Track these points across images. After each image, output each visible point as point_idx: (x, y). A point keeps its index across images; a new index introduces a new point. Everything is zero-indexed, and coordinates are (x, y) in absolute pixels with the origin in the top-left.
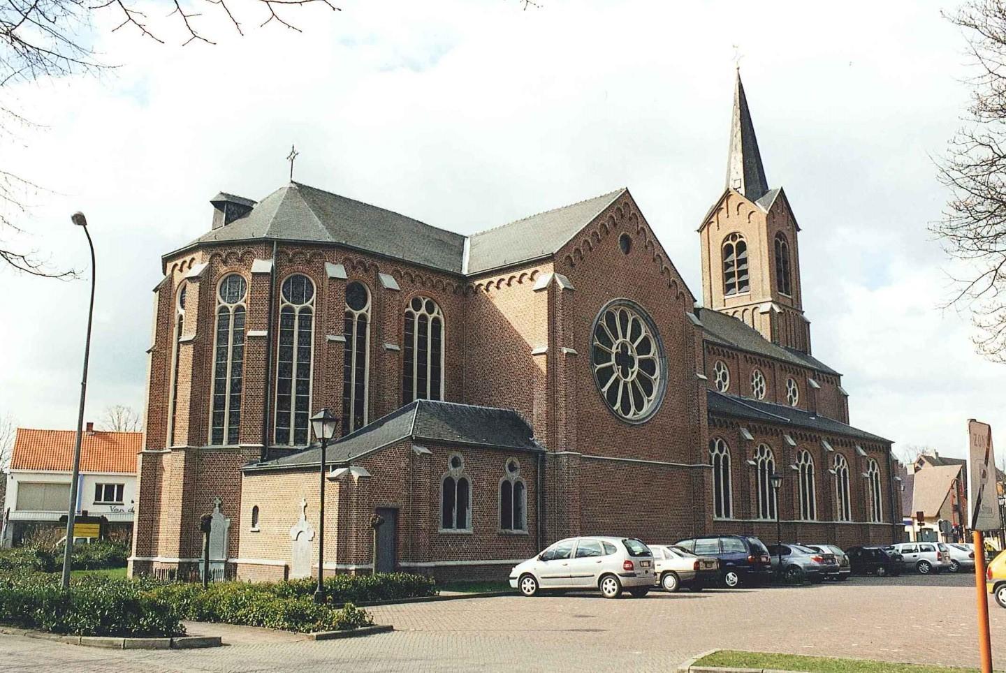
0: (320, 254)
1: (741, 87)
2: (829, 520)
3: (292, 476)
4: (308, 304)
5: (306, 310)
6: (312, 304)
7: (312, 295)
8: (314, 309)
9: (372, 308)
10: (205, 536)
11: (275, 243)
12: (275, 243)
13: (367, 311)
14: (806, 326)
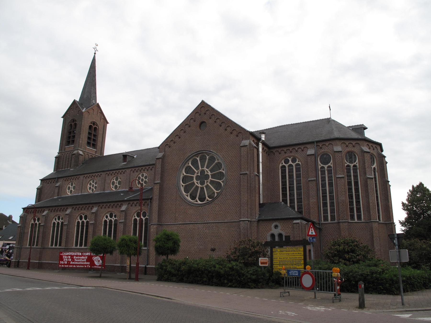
0: (331, 144)
1: (94, 57)
2: (393, 250)
3: (96, 286)
4: (355, 164)
5: (355, 166)
6: (331, 164)
7: (331, 160)
8: (358, 165)
9: (333, 162)
10: (289, 315)
11: (315, 142)
12: (315, 142)
13: (357, 163)
14: (379, 148)
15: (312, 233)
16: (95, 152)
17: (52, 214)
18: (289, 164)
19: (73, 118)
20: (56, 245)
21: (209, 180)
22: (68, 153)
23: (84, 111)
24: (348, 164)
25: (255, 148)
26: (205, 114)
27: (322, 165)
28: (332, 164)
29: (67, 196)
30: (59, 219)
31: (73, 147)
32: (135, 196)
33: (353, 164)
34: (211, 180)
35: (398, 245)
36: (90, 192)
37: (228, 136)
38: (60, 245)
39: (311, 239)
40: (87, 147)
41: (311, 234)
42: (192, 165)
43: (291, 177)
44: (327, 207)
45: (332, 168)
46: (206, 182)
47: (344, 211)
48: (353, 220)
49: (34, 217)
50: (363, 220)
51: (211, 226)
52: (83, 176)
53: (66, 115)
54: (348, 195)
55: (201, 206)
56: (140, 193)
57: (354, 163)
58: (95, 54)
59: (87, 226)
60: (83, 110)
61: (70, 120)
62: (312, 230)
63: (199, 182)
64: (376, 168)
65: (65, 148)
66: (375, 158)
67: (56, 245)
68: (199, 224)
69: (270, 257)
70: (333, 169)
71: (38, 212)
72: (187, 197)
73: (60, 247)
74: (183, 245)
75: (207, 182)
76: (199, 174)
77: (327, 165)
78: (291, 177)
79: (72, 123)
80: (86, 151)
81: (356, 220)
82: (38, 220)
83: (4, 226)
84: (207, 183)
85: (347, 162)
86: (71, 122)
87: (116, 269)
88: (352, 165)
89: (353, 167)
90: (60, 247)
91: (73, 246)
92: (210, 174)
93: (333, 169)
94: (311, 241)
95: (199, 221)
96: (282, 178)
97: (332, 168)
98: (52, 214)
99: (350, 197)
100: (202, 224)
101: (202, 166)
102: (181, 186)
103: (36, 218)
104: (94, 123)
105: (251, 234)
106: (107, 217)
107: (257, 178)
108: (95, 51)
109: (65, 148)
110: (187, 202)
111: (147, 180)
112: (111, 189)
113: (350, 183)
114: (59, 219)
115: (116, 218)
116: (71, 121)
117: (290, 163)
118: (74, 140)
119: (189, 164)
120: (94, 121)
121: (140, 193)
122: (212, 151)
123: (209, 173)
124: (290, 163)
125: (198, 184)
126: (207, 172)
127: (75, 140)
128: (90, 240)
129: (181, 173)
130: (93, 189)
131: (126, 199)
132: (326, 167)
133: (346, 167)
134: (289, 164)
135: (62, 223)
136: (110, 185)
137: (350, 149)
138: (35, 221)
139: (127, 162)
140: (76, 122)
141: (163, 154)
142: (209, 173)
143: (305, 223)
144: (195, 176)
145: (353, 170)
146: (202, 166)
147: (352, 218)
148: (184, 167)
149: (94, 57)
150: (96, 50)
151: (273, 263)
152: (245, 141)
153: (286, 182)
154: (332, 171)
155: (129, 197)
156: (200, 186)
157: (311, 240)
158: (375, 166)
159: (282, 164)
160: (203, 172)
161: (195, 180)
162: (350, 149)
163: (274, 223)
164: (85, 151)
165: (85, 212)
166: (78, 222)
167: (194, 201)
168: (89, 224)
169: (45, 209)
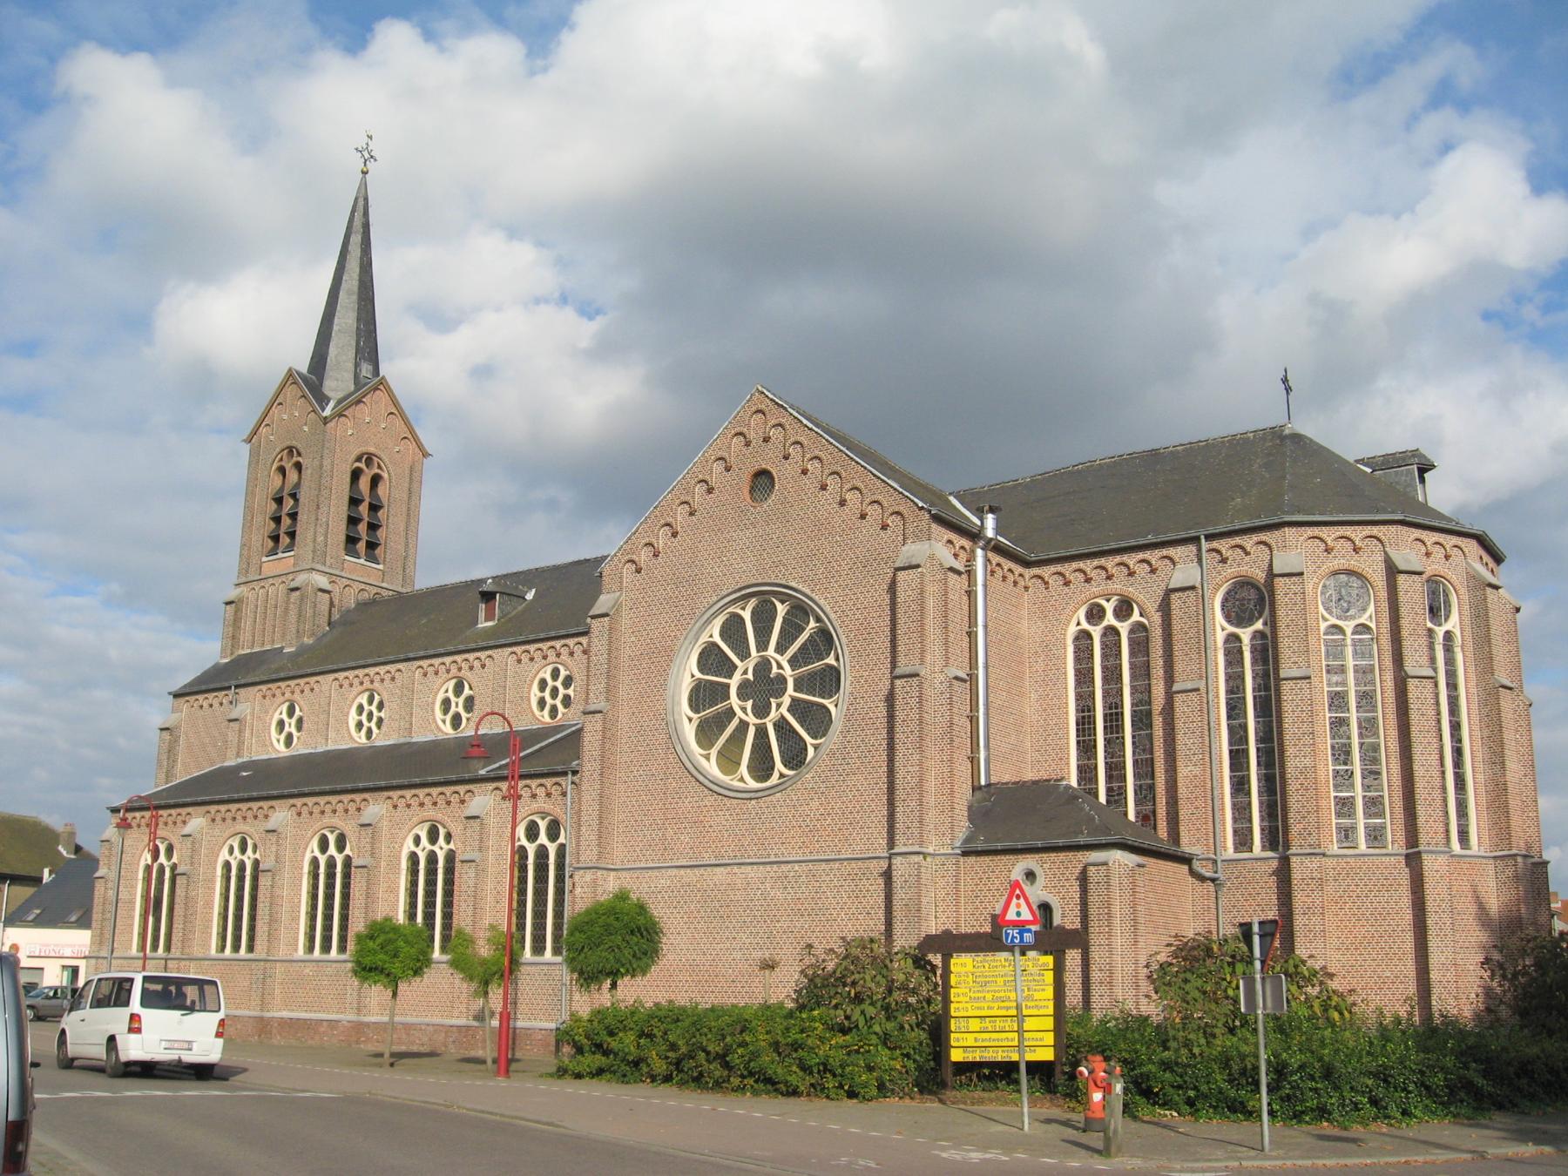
1: (364, 185)
15: (1018, 914)
16: (380, 573)
17: (217, 830)
18: (1105, 623)
19: (288, 443)
20: (236, 948)
21: (786, 701)
22: (273, 584)
23: (331, 415)
24: (1334, 621)
25: (950, 574)
26: (766, 440)
27: (1231, 629)
28: (1269, 623)
29: (274, 756)
30: (243, 850)
31: (292, 561)
32: (500, 768)
33: (1353, 623)
34: (794, 699)
35: (1263, 959)
36: (356, 742)
37: (851, 529)
38: (251, 949)
39: (1015, 935)
40: (347, 558)
41: (1016, 918)
42: (723, 640)
43: (1113, 675)
44: (1249, 794)
45: (1270, 639)
46: (774, 706)
47: (1309, 812)
48: (1352, 845)
49: (150, 841)
50: (1390, 847)
51: (792, 874)
52: (333, 678)
53: (261, 429)
54: (1333, 747)
55: (757, 798)
56: (508, 760)
57: (1360, 617)
58: (365, 173)
59: (347, 876)
60: (323, 410)
61: (278, 450)
62: (1018, 906)
63: (749, 704)
64: (1457, 632)
65: (262, 563)
66: (1453, 591)
67: (236, 948)
68: (749, 868)
69: (392, 1022)
70: (1270, 644)
71: (166, 824)
72: (703, 761)
73: (250, 956)
74: (677, 945)
75: (779, 706)
76: (750, 676)
77: (1249, 629)
78: (1113, 675)
79: (283, 463)
80: (343, 574)
81: (1363, 846)
82: (170, 850)
83: (46, 871)
84: (781, 708)
85: (1331, 613)
86: (281, 459)
87: (451, 1039)
88: (1347, 626)
89: (1353, 634)
90: (250, 956)
91: (296, 950)
92: (791, 676)
93: (1270, 644)
94: (1012, 941)
95: (749, 857)
96: (1078, 683)
97: (1270, 639)
98: (217, 830)
99: (1339, 755)
100: (761, 867)
101: (762, 645)
102: (686, 721)
103: (158, 842)
104: (369, 459)
105: (936, 906)
106: (417, 840)
107: (961, 689)
108: (366, 161)
109: (262, 563)
110: (706, 782)
111: (570, 692)
112: (438, 727)
113: (1341, 700)
114: (243, 850)
115: (452, 846)
116: (279, 456)
117: (1110, 619)
118: (295, 531)
119: (743, 609)
120: (372, 450)
121: (508, 760)
122: (793, 584)
123: (788, 671)
124: (1110, 619)
125: (747, 715)
126: (780, 666)
127: (300, 512)
128: (357, 925)
129: (685, 669)
130: (370, 731)
131: (482, 772)
132: (1246, 634)
133: (1324, 634)
134: (1105, 623)
135: (256, 863)
136: (433, 715)
137: (1342, 561)
138: (156, 856)
139: (497, 617)
140: (300, 459)
141: (616, 597)
142: (788, 671)
143: (1131, 865)
144: (734, 682)
145: (1354, 645)
146: (762, 645)
147: (1347, 837)
148: (697, 645)
149: (364, 185)
150: (367, 156)
151: (952, 1010)
152: (913, 547)
153: (1092, 695)
154: (1268, 650)
155: (497, 765)
156: (752, 719)
157: (1013, 937)
158: (1452, 625)
159: (1078, 624)
160: (763, 666)
161: (734, 700)
162: (1342, 561)
163: (1020, 863)
164: (337, 573)
165: (335, 821)
166: (315, 862)
167: (732, 780)
168: (353, 869)
169: (190, 810)
